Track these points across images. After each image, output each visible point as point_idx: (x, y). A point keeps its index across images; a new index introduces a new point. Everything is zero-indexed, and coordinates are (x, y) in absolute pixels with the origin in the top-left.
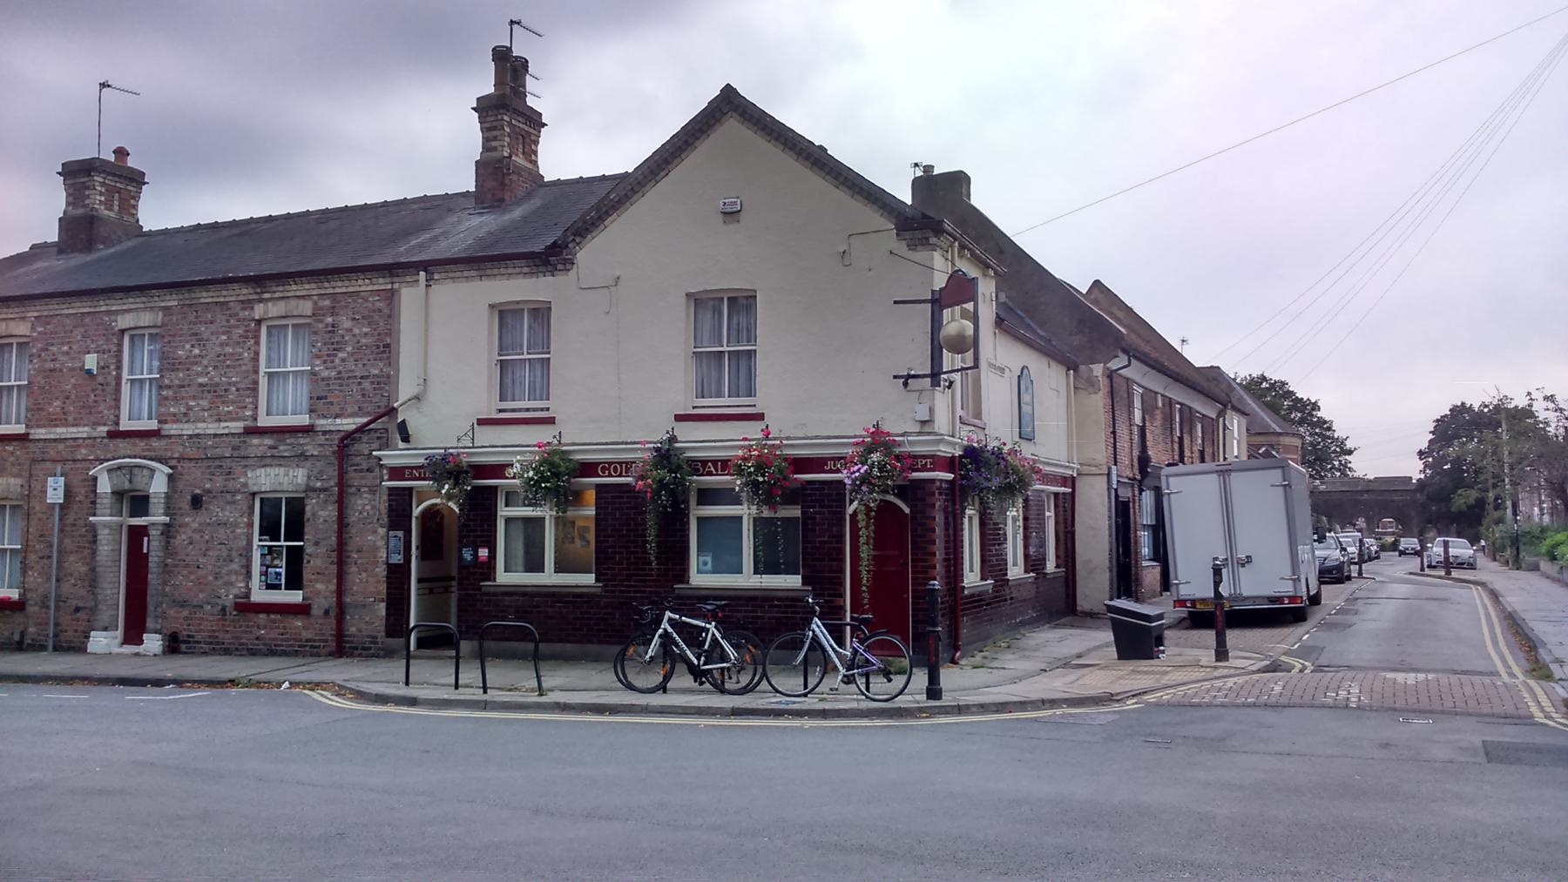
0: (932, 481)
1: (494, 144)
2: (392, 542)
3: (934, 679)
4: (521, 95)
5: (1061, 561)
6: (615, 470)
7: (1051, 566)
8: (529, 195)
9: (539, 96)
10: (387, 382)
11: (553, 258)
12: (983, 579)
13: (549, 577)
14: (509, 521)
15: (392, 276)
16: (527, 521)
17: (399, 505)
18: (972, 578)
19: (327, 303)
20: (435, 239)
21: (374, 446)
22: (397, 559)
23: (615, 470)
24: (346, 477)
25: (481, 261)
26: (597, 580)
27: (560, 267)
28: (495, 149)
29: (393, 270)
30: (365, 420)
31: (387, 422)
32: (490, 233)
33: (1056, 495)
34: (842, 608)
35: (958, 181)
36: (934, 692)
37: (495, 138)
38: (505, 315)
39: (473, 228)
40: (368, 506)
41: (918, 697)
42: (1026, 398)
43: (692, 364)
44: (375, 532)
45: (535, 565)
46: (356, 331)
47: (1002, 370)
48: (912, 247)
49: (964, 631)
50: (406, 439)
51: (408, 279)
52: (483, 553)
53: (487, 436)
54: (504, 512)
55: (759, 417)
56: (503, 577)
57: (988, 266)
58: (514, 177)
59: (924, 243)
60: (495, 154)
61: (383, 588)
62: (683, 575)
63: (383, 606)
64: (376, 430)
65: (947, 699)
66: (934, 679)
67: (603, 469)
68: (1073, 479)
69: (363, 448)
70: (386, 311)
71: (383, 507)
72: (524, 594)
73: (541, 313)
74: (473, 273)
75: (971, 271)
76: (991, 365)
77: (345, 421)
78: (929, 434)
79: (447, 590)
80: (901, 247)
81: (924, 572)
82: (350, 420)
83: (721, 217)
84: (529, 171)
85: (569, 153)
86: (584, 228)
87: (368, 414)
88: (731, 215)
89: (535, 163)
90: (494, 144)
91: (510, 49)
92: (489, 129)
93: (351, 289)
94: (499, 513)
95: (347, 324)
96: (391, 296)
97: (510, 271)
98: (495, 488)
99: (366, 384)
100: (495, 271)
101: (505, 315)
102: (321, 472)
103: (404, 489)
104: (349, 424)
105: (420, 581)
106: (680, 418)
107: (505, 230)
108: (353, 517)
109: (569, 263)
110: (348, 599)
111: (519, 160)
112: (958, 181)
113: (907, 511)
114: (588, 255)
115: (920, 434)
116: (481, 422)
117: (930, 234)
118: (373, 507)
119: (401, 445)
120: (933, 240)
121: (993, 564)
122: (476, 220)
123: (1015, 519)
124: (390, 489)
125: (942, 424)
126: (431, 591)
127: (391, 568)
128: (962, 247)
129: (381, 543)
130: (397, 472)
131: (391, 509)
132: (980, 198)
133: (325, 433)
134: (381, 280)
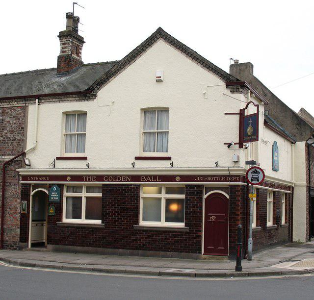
1: (65, 50)
3: (239, 264)
5: (288, 221)
7: (283, 222)
10: (22, 142)
11: (88, 94)
12: (274, 224)
13: (83, 221)
14: (67, 198)
16: (74, 198)
17: (26, 189)
21: (17, 167)
26: (185, 226)
27: (91, 97)
28: (65, 51)
30: (13, 157)
33: (286, 194)
35: (249, 66)
36: (238, 268)
37: (66, 48)
38: (68, 115)
42: (275, 154)
43: (142, 137)
51: (32, 102)
55: (169, 158)
56: (65, 220)
57: (262, 101)
58: (72, 63)
59: (237, 91)
60: (66, 54)
61: (19, 223)
62: (137, 221)
66: (239, 264)
67: (106, 178)
68: (293, 188)
69: (12, 167)
70: (23, 114)
71: (19, 191)
73: (83, 115)
74: (57, 100)
76: (263, 141)
77: (6, 157)
78: (239, 167)
79: (42, 225)
80: (228, 92)
81: (234, 220)
82: (8, 157)
84: (77, 60)
85: (89, 55)
86: (101, 83)
87: (15, 155)
89: (80, 57)
90: (65, 50)
91: (73, 14)
92: (63, 44)
93: (10, 106)
95: (8, 119)
96: (25, 109)
97: (71, 99)
99: (14, 143)
100: (65, 99)
101: (68, 115)
104: (7, 158)
105: (33, 221)
106: (137, 158)
110: (5, 227)
111: (74, 56)
112: (249, 66)
113: (228, 197)
114: (104, 93)
115: (234, 167)
116: (58, 158)
117: (239, 87)
118: (16, 191)
120: (241, 90)
121: (262, 219)
124: (22, 184)
126: (37, 225)
127: (22, 216)
128: (252, 93)
130: (25, 178)
131: (22, 192)
132: (257, 73)
134: (21, 102)
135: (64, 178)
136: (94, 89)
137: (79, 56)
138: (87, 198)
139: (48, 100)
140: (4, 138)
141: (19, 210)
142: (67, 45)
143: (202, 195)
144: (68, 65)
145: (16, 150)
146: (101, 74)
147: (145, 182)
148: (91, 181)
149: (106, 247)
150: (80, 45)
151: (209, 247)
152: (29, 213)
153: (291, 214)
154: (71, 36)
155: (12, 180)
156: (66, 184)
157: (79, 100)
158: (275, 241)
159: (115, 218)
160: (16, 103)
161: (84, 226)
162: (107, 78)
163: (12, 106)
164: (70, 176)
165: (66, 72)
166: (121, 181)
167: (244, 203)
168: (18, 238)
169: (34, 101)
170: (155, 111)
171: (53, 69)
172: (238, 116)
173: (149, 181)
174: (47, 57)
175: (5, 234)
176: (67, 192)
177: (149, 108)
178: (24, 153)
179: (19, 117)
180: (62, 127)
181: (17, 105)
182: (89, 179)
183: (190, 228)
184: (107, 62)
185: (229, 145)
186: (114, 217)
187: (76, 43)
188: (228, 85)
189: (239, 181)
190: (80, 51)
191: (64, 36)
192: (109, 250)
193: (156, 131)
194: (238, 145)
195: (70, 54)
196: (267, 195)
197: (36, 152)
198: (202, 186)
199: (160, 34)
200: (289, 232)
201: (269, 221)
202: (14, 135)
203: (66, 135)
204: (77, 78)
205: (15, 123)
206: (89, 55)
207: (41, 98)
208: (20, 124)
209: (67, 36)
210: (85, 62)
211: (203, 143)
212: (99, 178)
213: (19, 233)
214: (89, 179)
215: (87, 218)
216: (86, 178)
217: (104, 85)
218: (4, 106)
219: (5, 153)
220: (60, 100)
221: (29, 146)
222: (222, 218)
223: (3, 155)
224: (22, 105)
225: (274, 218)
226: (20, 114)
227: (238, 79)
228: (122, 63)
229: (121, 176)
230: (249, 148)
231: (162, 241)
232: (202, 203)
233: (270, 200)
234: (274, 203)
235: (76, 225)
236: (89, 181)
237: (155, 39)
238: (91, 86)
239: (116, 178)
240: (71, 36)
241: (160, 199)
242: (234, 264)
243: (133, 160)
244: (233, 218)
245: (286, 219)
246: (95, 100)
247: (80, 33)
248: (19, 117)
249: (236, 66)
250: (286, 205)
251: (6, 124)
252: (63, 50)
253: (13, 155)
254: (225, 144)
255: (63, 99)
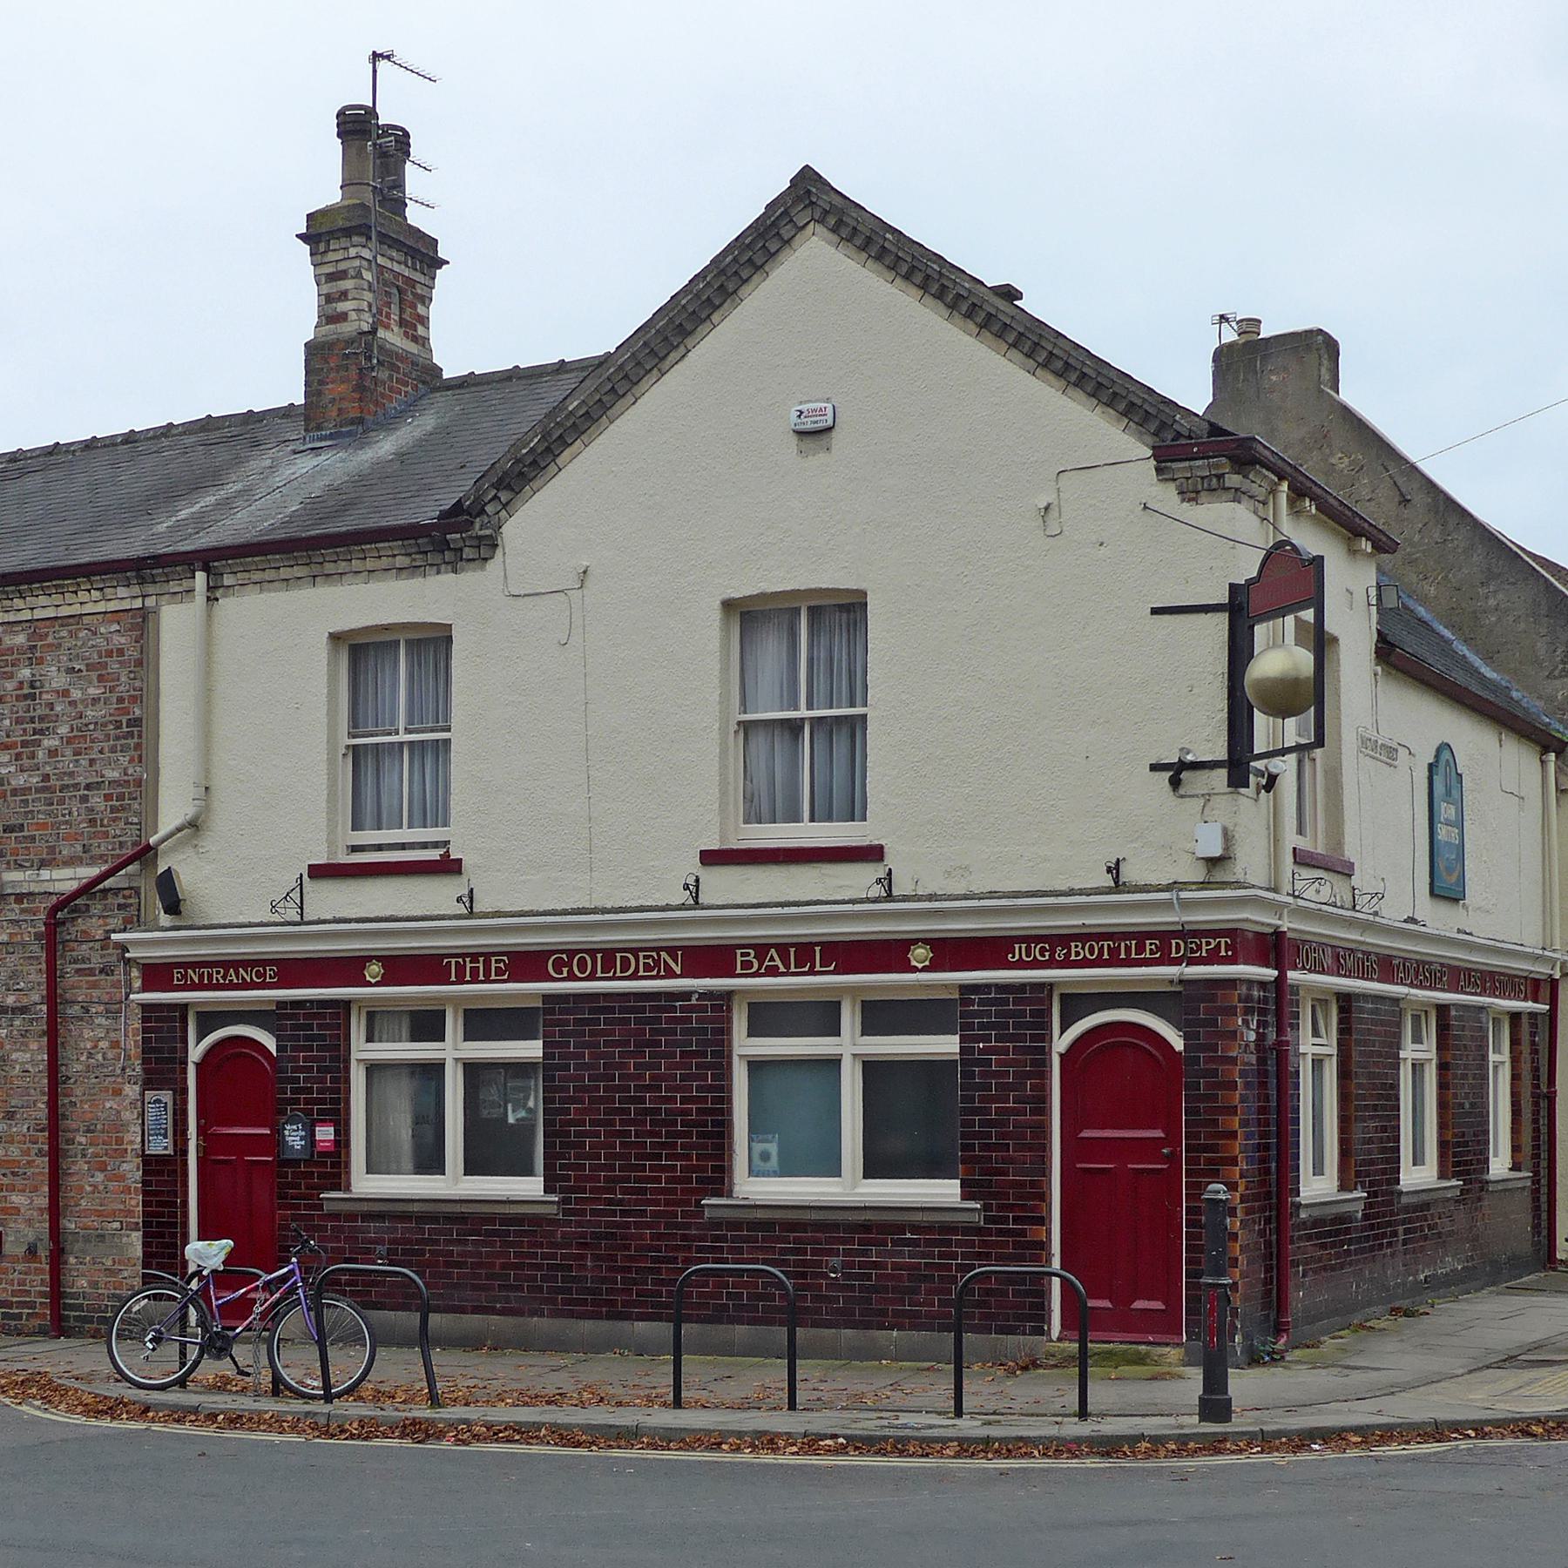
0: (1231, 983)
1: (342, 306)
2: (151, 1112)
3: (1215, 1383)
4: (398, 205)
6: (582, 965)
7: (1499, 1165)
8: (411, 408)
9: (429, 201)
10: (138, 792)
11: (456, 537)
12: (1343, 1187)
13: (454, 1184)
15: (142, 581)
17: (164, 1029)
18: (1318, 1186)
19: (21, 639)
20: (226, 505)
21: (116, 922)
22: (161, 1146)
23: (582, 965)
24: (62, 983)
25: (310, 548)
26: (964, 1197)
28: (342, 317)
29: (144, 569)
30: (94, 871)
31: (141, 873)
32: (333, 490)
33: (1515, 1017)
34: (1044, 1246)
35: (1316, 350)
36: (1215, 1405)
37: (344, 296)
38: (361, 651)
39: (296, 481)
40: (106, 1040)
41: (1186, 1420)
42: (1446, 811)
43: (736, 745)
44: (118, 1092)
45: (430, 1160)
46: (76, 694)
47: (1391, 752)
48: (1190, 494)
49: (1298, 1297)
50: (173, 906)
51: (174, 586)
52: (325, 1133)
53: (330, 900)
54: (362, 1050)
55: (873, 854)
56: (366, 1184)
58: (383, 374)
61: (136, 1202)
62: (719, 1180)
63: (136, 1238)
64: (116, 891)
65: (1240, 1423)
66: (1215, 1383)
67: (558, 966)
68: (1554, 984)
71: (132, 1043)
72: (405, 1217)
73: (432, 644)
74: (299, 571)
75: (1310, 539)
77: (58, 874)
78: (1224, 885)
82: (67, 872)
83: (794, 439)
84: (404, 357)
85: (467, 332)
86: (520, 474)
87: (103, 858)
88: (815, 435)
89: (424, 342)
90: (342, 306)
91: (371, 112)
92: (332, 277)
94: (354, 1055)
95: (58, 680)
96: (142, 623)
97: (370, 564)
98: (345, 1005)
99: (97, 800)
101: (361, 651)
102: (14, 975)
103: (172, 1007)
104: (65, 879)
106: (710, 858)
107: (363, 481)
108: (74, 1066)
109: (488, 546)
110: (69, 1224)
111: (393, 337)
112: (1316, 350)
113: (1178, 1044)
114: (528, 527)
115: (1204, 885)
118: (115, 1044)
119: (165, 920)
120: (1233, 480)
121: (1370, 1161)
122: (306, 464)
123: (1418, 1067)
124: (146, 1007)
125: (1251, 864)
127: (151, 1165)
129: (129, 1115)
130: (157, 975)
131: (147, 1048)
133: (20, 898)
134: (122, 592)
135: (348, 969)
136: (482, 512)
137: (415, 339)
138: (873, 1070)
139: (257, 576)
140: (46, 778)
141: (133, 1136)
142: (347, 284)
143: (1046, 1037)
144: (360, 388)
145: (106, 834)
146: (524, 419)
147: (756, 975)
148: (487, 981)
149: (572, 1315)
150: (417, 276)
151: (1139, 1304)
152: (185, 1152)
153: (1543, 1121)
154: (371, 231)
155: (94, 985)
156: (744, 992)
157: (413, 570)
158: (1452, 1263)
159: (612, 1168)
160: (95, 594)
161: (458, 1208)
162: (548, 449)
163: (76, 610)
164: (926, 941)
165: (352, 422)
166: (635, 976)
167: (1262, 1073)
168: (132, 1274)
169: (186, 584)
170: (797, 611)
171: (288, 412)
172: (1223, 619)
173: (773, 972)
174: (249, 345)
175: (72, 1260)
176: (369, 1039)
177: (763, 596)
178: (148, 848)
179: (114, 666)
180: (725, 669)
181: (101, 607)
182: (475, 971)
183: (986, 1208)
184: (170, 425)
185: (1177, 772)
186: (619, 1168)
187: (396, 267)
188: (1165, 458)
189: (1232, 961)
190: (421, 309)
191: (333, 234)
192: (587, 1326)
193: (803, 713)
194: (1222, 774)
195: (366, 327)
196: (1399, 1025)
197: (208, 843)
198: (1047, 988)
199: (809, 202)
200: (1537, 1216)
201: (1318, 1169)
202: (92, 762)
203: (747, 727)
204: (400, 449)
205: (95, 701)
206: (467, 332)
207: (219, 563)
208: (120, 700)
209: (348, 232)
210: (451, 370)
211: (1042, 767)
212: (526, 964)
213: (139, 1253)
214: (475, 971)
215: (472, 1168)
216: (461, 969)
217: (535, 484)
218: (39, 614)
219: (52, 850)
220: (316, 569)
221: (172, 812)
222: (1133, 1155)
223: (43, 864)
224: (126, 605)
225: (1443, 1145)
226: (121, 652)
227: (1268, 420)
228: (621, 367)
229: (635, 952)
230: (1287, 784)
231: (846, 1276)
232: (1042, 1073)
233: (1418, 1050)
234: (1443, 1067)
235: (416, 1208)
236: (475, 980)
237: (786, 232)
238: (466, 497)
239: (608, 959)
240: (371, 231)
241: (434, 1071)
242: (1193, 1383)
243: (693, 865)
244: (1207, 1148)
245: (1516, 1148)
246: (490, 565)
247: (415, 216)
248: (114, 666)
249: (1245, 358)
250: (1515, 1077)
251: (51, 706)
252: (329, 309)
253: (93, 861)
254: (1154, 768)
255: (329, 568)
